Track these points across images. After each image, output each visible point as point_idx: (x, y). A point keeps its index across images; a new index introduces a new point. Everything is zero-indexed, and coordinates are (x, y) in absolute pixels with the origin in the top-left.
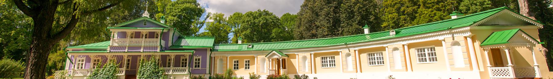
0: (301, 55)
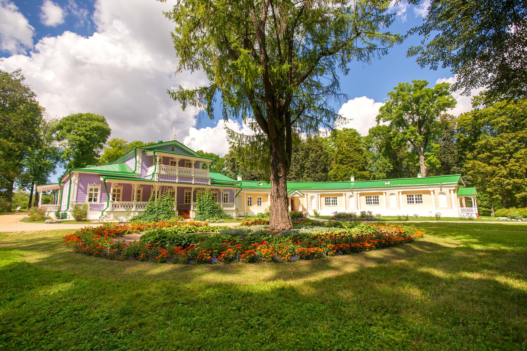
0: (310, 195)
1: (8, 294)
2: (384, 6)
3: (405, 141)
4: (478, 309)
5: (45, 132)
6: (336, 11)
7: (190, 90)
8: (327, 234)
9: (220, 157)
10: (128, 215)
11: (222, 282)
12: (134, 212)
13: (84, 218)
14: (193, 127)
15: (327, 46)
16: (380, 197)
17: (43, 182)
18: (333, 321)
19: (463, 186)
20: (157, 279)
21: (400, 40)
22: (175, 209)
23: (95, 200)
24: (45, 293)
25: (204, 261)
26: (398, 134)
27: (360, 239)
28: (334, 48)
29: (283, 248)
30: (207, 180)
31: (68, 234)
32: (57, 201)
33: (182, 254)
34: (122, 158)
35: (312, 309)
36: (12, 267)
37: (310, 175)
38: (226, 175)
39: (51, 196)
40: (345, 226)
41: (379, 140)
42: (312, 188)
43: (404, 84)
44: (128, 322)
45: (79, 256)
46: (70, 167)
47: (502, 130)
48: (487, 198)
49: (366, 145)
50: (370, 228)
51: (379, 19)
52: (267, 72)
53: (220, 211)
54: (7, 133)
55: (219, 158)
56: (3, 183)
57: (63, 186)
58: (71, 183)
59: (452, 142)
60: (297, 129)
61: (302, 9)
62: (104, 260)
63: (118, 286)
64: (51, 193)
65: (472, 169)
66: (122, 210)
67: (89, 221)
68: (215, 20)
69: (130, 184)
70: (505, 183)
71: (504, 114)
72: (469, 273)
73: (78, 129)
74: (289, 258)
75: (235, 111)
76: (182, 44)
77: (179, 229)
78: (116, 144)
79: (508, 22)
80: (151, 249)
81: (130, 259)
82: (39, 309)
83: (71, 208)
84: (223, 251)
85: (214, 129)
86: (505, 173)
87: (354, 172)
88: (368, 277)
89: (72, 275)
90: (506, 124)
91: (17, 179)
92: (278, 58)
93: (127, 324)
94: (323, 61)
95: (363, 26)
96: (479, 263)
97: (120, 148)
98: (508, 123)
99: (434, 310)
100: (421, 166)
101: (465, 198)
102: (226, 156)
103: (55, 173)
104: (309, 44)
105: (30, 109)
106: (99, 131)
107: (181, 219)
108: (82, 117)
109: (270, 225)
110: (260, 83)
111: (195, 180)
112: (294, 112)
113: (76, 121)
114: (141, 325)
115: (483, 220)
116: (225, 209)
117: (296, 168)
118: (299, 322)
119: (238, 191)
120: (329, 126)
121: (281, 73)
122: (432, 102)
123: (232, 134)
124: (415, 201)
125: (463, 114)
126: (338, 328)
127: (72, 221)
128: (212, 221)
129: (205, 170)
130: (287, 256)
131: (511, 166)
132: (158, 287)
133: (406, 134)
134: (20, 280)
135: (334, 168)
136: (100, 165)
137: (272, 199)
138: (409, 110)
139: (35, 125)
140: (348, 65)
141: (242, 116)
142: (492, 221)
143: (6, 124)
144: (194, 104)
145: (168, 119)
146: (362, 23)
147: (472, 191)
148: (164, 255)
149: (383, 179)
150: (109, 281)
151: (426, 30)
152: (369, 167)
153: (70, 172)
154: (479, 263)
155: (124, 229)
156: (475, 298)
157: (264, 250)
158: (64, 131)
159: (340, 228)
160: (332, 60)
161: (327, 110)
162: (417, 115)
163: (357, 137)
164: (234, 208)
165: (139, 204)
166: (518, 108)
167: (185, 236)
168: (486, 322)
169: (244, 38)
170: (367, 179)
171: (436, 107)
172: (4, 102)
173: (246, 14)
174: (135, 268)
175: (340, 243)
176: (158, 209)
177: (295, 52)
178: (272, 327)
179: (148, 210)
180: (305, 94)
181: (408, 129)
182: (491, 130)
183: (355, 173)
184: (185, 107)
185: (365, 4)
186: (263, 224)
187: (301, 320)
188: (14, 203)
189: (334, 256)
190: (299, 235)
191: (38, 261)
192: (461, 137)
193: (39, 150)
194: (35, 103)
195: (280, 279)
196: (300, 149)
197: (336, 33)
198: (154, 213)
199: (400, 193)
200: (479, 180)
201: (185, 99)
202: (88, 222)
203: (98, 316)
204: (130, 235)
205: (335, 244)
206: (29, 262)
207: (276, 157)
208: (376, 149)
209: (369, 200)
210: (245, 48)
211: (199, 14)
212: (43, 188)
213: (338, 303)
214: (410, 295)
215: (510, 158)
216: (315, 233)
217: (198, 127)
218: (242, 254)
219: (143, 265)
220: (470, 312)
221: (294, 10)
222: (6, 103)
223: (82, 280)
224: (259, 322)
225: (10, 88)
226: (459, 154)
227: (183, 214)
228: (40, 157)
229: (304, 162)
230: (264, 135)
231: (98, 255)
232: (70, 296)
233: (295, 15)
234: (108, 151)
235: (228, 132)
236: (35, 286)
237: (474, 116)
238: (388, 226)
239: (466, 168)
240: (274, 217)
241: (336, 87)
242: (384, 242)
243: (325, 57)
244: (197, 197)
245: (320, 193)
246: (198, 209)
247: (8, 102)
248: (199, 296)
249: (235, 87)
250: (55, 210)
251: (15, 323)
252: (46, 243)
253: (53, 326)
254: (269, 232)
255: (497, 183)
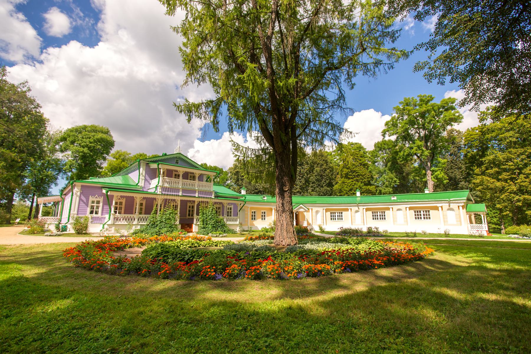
0: (315, 209)
1: (5, 311)
2: (389, 22)
3: (411, 155)
4: (497, 332)
5: (48, 144)
6: (342, 27)
7: (196, 103)
8: (334, 250)
9: (224, 170)
10: (130, 228)
11: (227, 299)
12: (136, 226)
13: (85, 231)
14: (198, 139)
15: (333, 61)
16: (387, 212)
17: (44, 193)
18: (345, 343)
19: (471, 202)
20: (159, 297)
21: (406, 55)
22: (178, 222)
23: (96, 213)
24: (43, 310)
25: (208, 277)
26: (405, 148)
27: (369, 255)
28: (340, 63)
29: (290, 264)
30: (211, 193)
31: (69, 247)
32: (58, 213)
33: (186, 270)
34: (125, 170)
35: (322, 330)
36: (9, 282)
37: (314, 189)
38: (229, 188)
39: (51, 208)
40: (352, 242)
41: (385, 154)
42: (318, 202)
43: (409, 99)
44: (129, 342)
45: (78, 271)
46: (72, 178)
47: (510, 145)
48: (497, 214)
49: (372, 159)
50: (377, 244)
51: (384, 35)
52: (273, 86)
53: (224, 225)
54: (11, 144)
55: (223, 171)
56: (3, 194)
57: (65, 198)
58: (72, 195)
59: (460, 157)
60: (302, 142)
61: (309, 24)
62: (104, 275)
63: (119, 304)
64: (52, 205)
65: (481, 185)
66: (123, 223)
67: (89, 234)
68: (222, 34)
69: (133, 197)
70: (515, 199)
71: (512, 129)
72: (484, 293)
73: (82, 141)
74: (295, 275)
75: (241, 124)
76: (190, 58)
77: (181, 243)
78: (120, 156)
79: (515, 39)
80: (154, 264)
81: (131, 275)
82: (36, 327)
83: (71, 221)
84: (227, 267)
85: (219, 141)
86: (515, 190)
87: (360, 187)
88: (379, 296)
89: (72, 291)
90: (514, 139)
91: (18, 191)
92: (285, 72)
93: (128, 344)
94: (329, 75)
95: (368, 42)
96: (494, 283)
97: (123, 160)
98: (516, 139)
99: (450, 334)
100: (428, 181)
101: (474, 214)
102: (230, 169)
103: (56, 184)
104: (315, 59)
105: (35, 121)
106: (103, 143)
107: (184, 233)
108: (87, 129)
109: (275, 241)
110: (266, 97)
111: (199, 194)
112: (300, 126)
113: (80, 133)
114: (143, 345)
115: (494, 238)
116: (228, 223)
117: (301, 182)
118: (309, 344)
119: (242, 205)
120: (335, 140)
121: (288, 87)
122: (438, 117)
123: (237, 147)
124: (422, 216)
125: (470, 129)
126: (350, 351)
127: (72, 234)
128: (215, 235)
129: (209, 183)
130: (293, 272)
131: (521, 182)
132: (160, 305)
133: (412, 148)
134: (17, 295)
135: (339, 182)
136: (102, 176)
137: (277, 213)
138: (415, 124)
139: (39, 136)
140: (354, 80)
141: (248, 128)
142: (503, 238)
143: (10, 135)
144: (200, 116)
145: (173, 131)
146: (367, 39)
147: (482, 208)
148: (166, 271)
149: (389, 194)
150: (109, 298)
151: (432, 46)
152: (375, 182)
153: (72, 184)
154: (494, 283)
155: (126, 243)
156: (493, 320)
157: (269, 267)
158: (68, 143)
159: (347, 244)
160: (338, 75)
161: (333, 124)
162: (423, 130)
163: (362, 151)
164: (238, 223)
165: (141, 217)
166: (525, 124)
167: (188, 251)
168: (506, 347)
169: (251, 52)
170: (373, 194)
171: (442, 121)
172: (9, 113)
173: (253, 29)
174: (137, 284)
175: (348, 260)
176: (160, 223)
177: (301, 66)
178: (280, 349)
179: (150, 223)
180: (311, 108)
181: (414, 143)
182: (498, 145)
183: (361, 188)
184: (191, 120)
185: (371, 20)
186: (268, 239)
187: (310, 342)
188: (13, 214)
189: (342, 273)
190: (305, 251)
191: (36, 276)
192: (469, 152)
193: (42, 161)
194: (40, 114)
195: (287, 297)
196: (304, 163)
197: (342, 49)
198: (156, 226)
199: (408, 209)
200: (488, 196)
201: (191, 112)
202: (89, 235)
203: (98, 335)
204: (131, 249)
205: (343, 260)
206: (28, 276)
207: (281, 170)
208: (382, 164)
209: (375, 215)
210: (251, 62)
211: (207, 28)
212: (44, 200)
213: (349, 324)
214: (424, 317)
215: (519, 174)
216: (321, 248)
217: (203, 139)
218: (247, 270)
219: (144, 281)
220: (488, 336)
221: (300, 26)
222: (11, 114)
223: (82, 297)
224: (267, 344)
225: (16, 99)
226: (466, 169)
227: (186, 228)
228: (43, 168)
229: (309, 176)
230: (270, 148)
231: (99, 270)
232: (68, 313)
233: (302, 31)
234: (111, 163)
235: (234, 145)
236: (32, 302)
237: (481, 131)
238: (396, 242)
239: (474, 183)
240: (279, 232)
241: (342, 101)
242: (393, 259)
243: (330, 71)
244: (201, 211)
245: (325, 208)
246: (201, 223)
247: (13, 113)
248: (203, 314)
249: (241, 100)
250: (56, 223)
251: (11, 342)
252: (45, 257)
253: (51, 346)
254: (273, 247)
255: (507, 199)
